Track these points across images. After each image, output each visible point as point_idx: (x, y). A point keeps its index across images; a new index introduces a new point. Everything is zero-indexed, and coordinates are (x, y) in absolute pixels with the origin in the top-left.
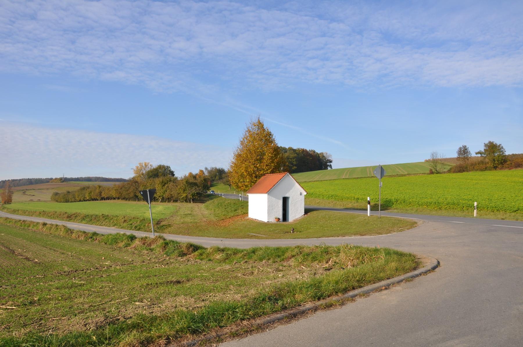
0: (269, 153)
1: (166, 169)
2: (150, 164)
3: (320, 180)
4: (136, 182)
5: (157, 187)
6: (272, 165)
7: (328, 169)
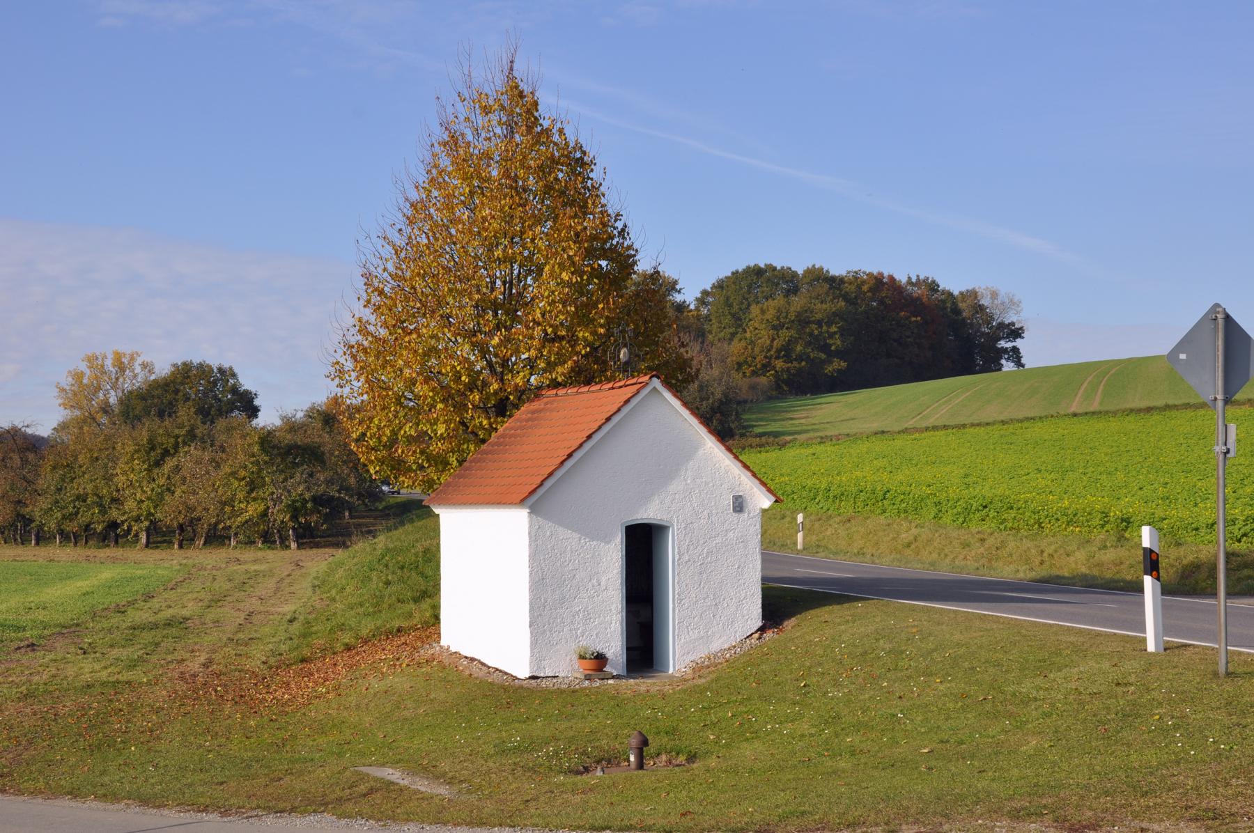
0: (562, 266)
1: (215, 383)
2: (139, 361)
3: (953, 424)
4: (28, 449)
5: (124, 473)
6: (581, 334)
7: (1004, 369)
